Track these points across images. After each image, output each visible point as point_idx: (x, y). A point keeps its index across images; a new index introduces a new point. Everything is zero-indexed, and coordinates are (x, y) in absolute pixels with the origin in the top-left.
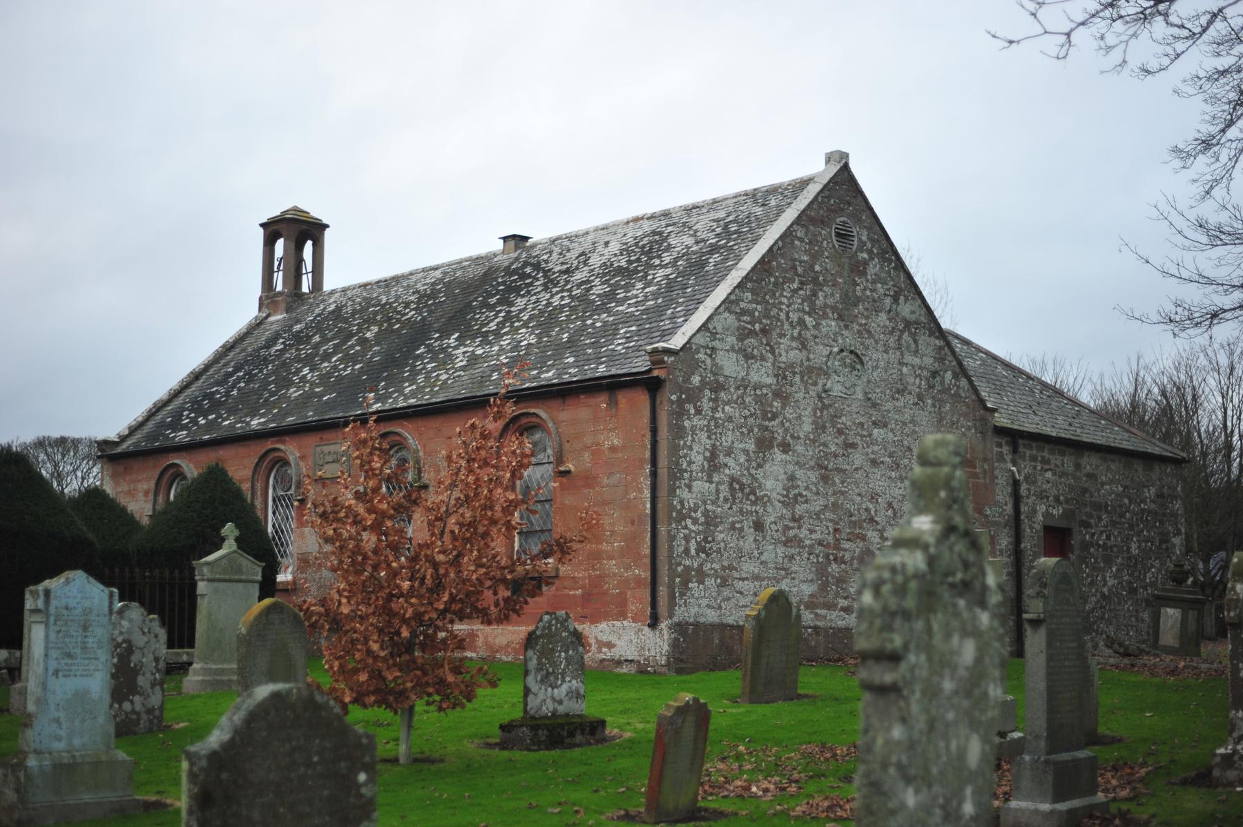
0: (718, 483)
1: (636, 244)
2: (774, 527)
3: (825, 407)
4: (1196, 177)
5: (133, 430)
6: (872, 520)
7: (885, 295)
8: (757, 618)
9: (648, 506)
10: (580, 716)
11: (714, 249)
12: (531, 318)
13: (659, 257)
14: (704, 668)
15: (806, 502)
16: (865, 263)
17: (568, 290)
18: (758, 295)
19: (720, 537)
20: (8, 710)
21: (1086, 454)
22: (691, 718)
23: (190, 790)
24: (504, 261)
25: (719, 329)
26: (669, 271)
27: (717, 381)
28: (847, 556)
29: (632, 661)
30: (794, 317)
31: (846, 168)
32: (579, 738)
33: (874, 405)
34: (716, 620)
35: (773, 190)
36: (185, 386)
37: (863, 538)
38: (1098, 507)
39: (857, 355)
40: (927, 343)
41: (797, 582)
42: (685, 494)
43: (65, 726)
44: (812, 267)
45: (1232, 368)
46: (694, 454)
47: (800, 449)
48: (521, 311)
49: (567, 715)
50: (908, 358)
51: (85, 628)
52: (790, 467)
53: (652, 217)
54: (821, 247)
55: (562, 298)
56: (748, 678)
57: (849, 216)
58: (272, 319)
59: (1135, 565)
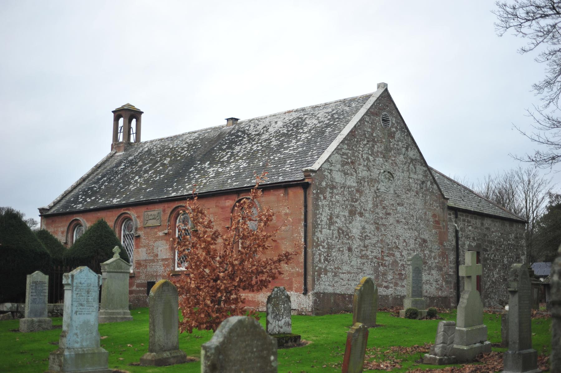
0: (333, 230)
1: (290, 123)
2: (356, 250)
3: (377, 197)
4: (543, 97)
5: (55, 204)
6: (397, 247)
7: (403, 147)
8: (360, 290)
9: (303, 240)
10: (289, 334)
11: (328, 126)
12: (244, 155)
13: (302, 129)
14: (327, 313)
15: (370, 239)
16: (394, 133)
17: (260, 143)
18: (350, 146)
19: (334, 254)
20: (18, 330)
21: (486, 219)
22: (361, 334)
23: (205, 363)
24: (227, 129)
25: (334, 161)
26: (307, 135)
27: (332, 185)
28: (387, 263)
29: (295, 310)
30: (365, 156)
31: (386, 90)
32: (290, 344)
33: (398, 196)
34: (332, 291)
35: (353, 100)
36: (79, 184)
37: (393, 255)
38: (491, 242)
39: (391, 174)
40: (420, 169)
41: (366, 274)
42: (319, 235)
43: (80, 336)
44: (372, 134)
45: (529, 181)
46: (323, 217)
47: (367, 215)
48: (238, 152)
49: (284, 333)
50: (412, 175)
51: (88, 292)
52: (363, 223)
53: (297, 111)
54: (376, 125)
55: (258, 146)
56: (356, 317)
57: (388, 112)
58: (117, 154)
59: (506, 268)
